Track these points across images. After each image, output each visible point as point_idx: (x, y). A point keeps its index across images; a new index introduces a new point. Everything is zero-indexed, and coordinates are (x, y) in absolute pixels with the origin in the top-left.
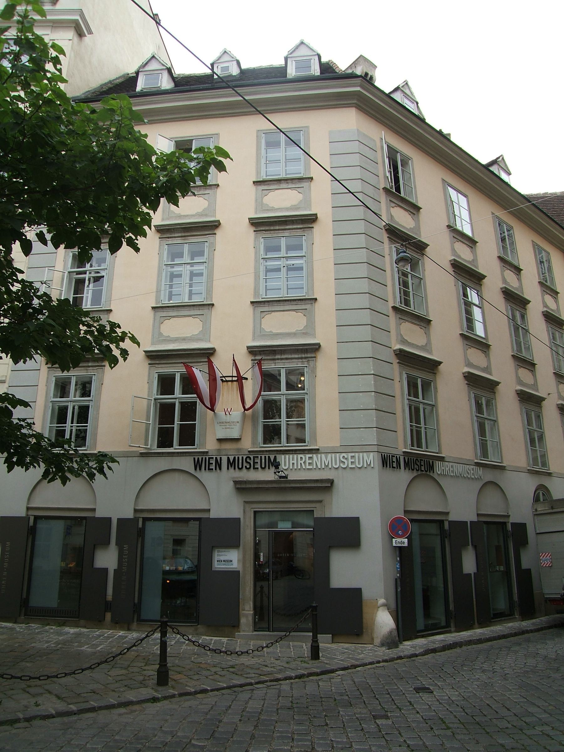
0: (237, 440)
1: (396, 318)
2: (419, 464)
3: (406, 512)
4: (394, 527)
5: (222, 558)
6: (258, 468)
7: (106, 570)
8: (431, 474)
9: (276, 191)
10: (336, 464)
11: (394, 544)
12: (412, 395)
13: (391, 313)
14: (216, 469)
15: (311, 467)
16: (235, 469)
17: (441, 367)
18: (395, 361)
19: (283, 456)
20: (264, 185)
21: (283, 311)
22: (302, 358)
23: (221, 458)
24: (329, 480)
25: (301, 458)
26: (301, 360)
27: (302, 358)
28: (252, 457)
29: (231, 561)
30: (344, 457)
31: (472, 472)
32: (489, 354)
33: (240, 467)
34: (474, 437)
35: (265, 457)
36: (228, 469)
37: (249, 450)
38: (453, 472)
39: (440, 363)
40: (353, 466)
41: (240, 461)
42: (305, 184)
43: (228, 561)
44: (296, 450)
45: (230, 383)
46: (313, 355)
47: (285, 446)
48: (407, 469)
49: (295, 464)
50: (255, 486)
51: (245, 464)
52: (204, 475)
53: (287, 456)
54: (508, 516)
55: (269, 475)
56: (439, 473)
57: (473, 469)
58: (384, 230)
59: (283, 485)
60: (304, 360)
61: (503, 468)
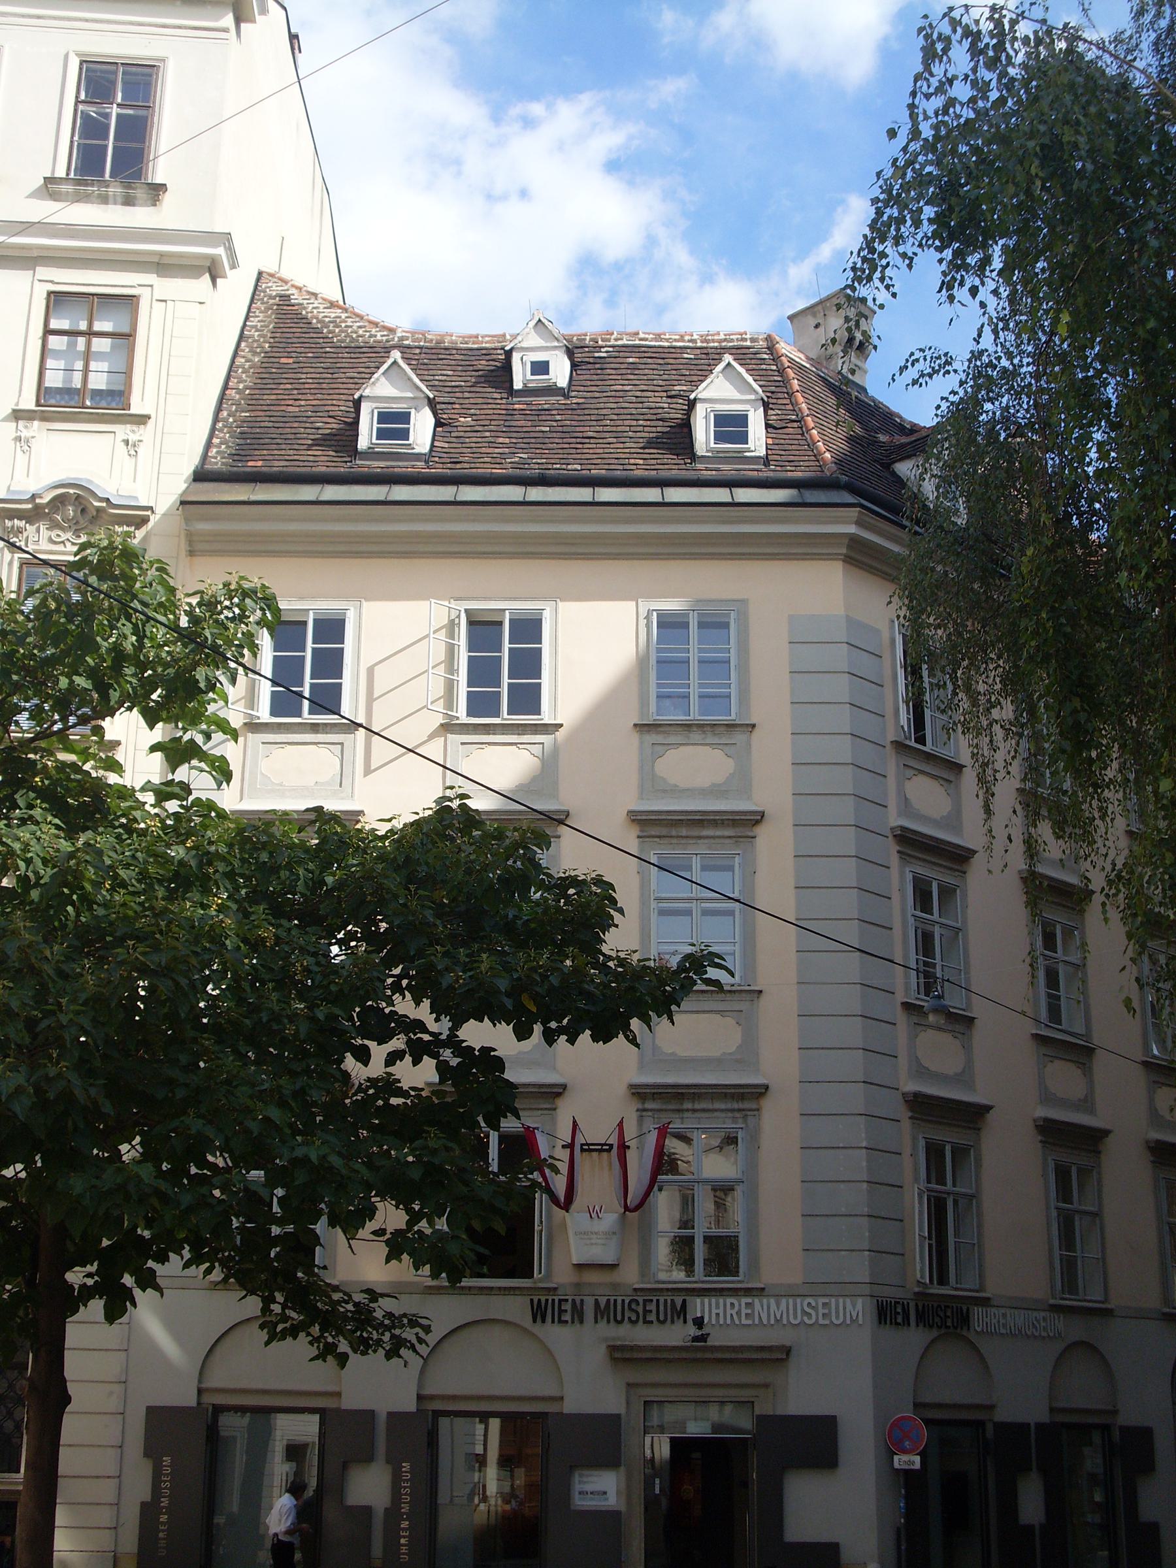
0: (613, 1267)
1: (898, 765)
2: (942, 1314)
3: (917, 1405)
4: (893, 1439)
5: (588, 1487)
6: (652, 1322)
7: (367, 1511)
8: (964, 1333)
9: (682, 748)
10: (795, 1317)
11: (896, 1465)
12: (933, 1180)
13: (901, 1017)
14: (573, 1322)
15: (749, 1322)
16: (608, 1321)
17: (991, 1116)
18: (904, 1114)
19: (698, 1300)
20: (658, 733)
21: (697, 1012)
22: (732, 1110)
23: (582, 1301)
24: (783, 1346)
25: (732, 1304)
26: (730, 1115)
27: (732, 1110)
28: (640, 1300)
29: (605, 1493)
30: (809, 1304)
31: (1043, 1324)
32: (1090, 1068)
33: (619, 1318)
34: (1051, 1250)
35: (666, 1301)
36: (596, 1322)
37: (636, 1286)
38: (1004, 1325)
39: (988, 1108)
40: (827, 1322)
41: (619, 1307)
42: (739, 738)
43: (598, 1493)
44: (722, 1289)
45: (595, 1154)
46: (754, 1106)
47: (703, 1282)
48: (921, 1325)
49: (721, 1315)
50: (648, 1355)
51: (627, 1314)
52: (557, 1335)
53: (706, 1300)
54: (1115, 1412)
55: (676, 1335)
56: (979, 1329)
57: (1044, 1319)
58: (891, 838)
59: (699, 1355)
60: (737, 1115)
61: (1108, 1313)
